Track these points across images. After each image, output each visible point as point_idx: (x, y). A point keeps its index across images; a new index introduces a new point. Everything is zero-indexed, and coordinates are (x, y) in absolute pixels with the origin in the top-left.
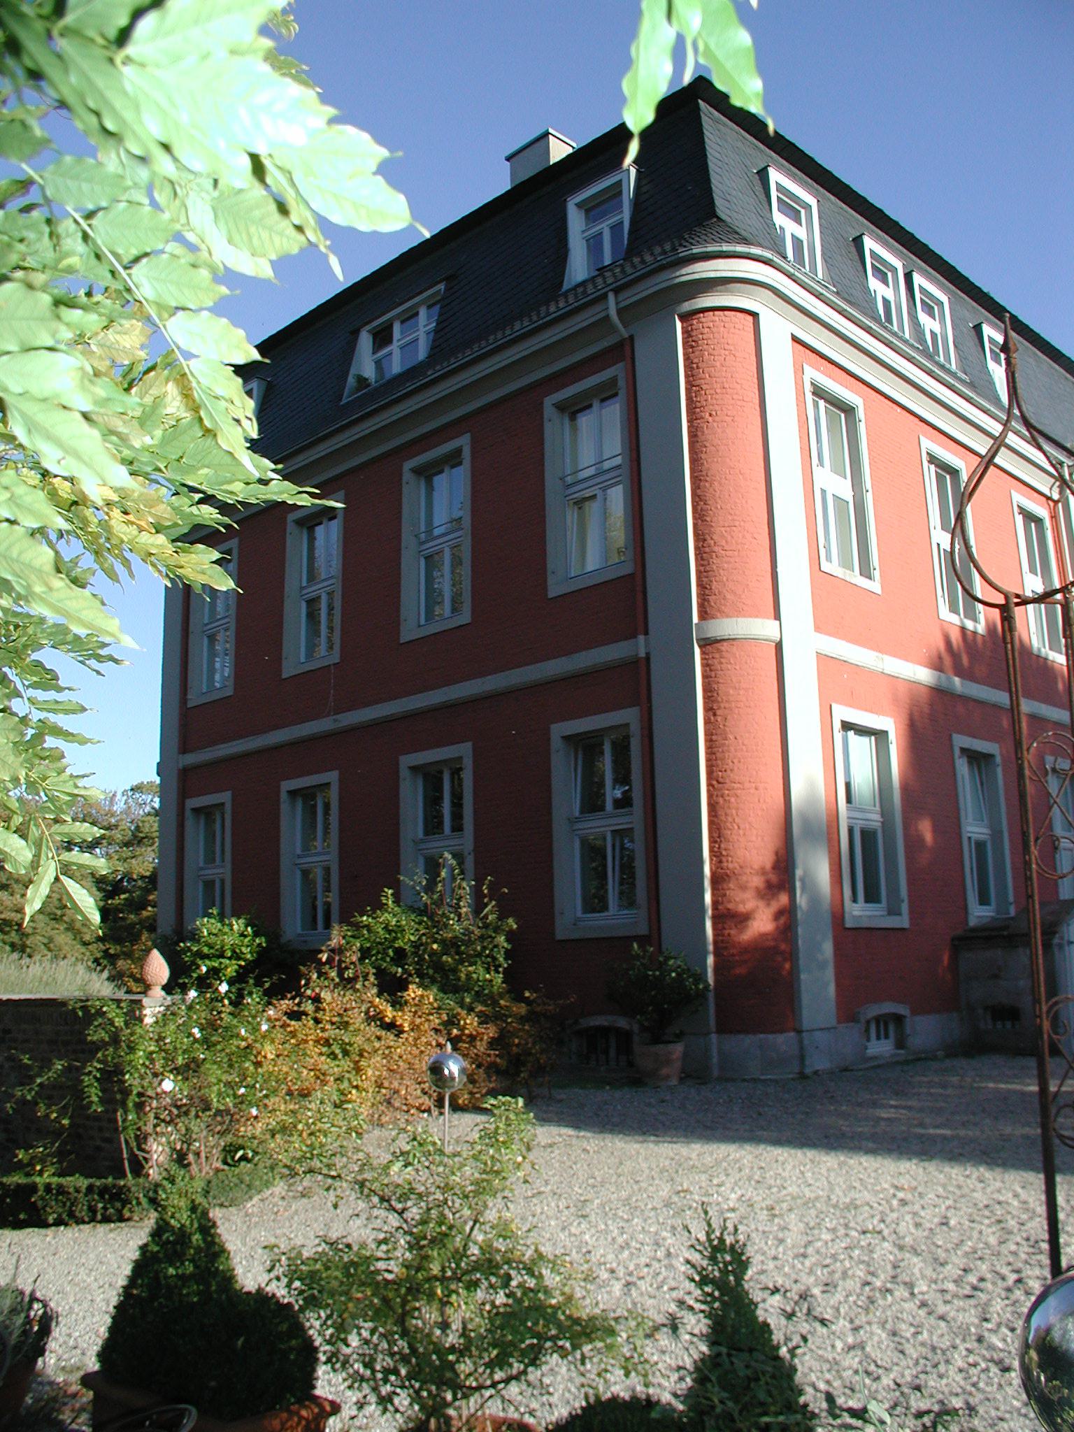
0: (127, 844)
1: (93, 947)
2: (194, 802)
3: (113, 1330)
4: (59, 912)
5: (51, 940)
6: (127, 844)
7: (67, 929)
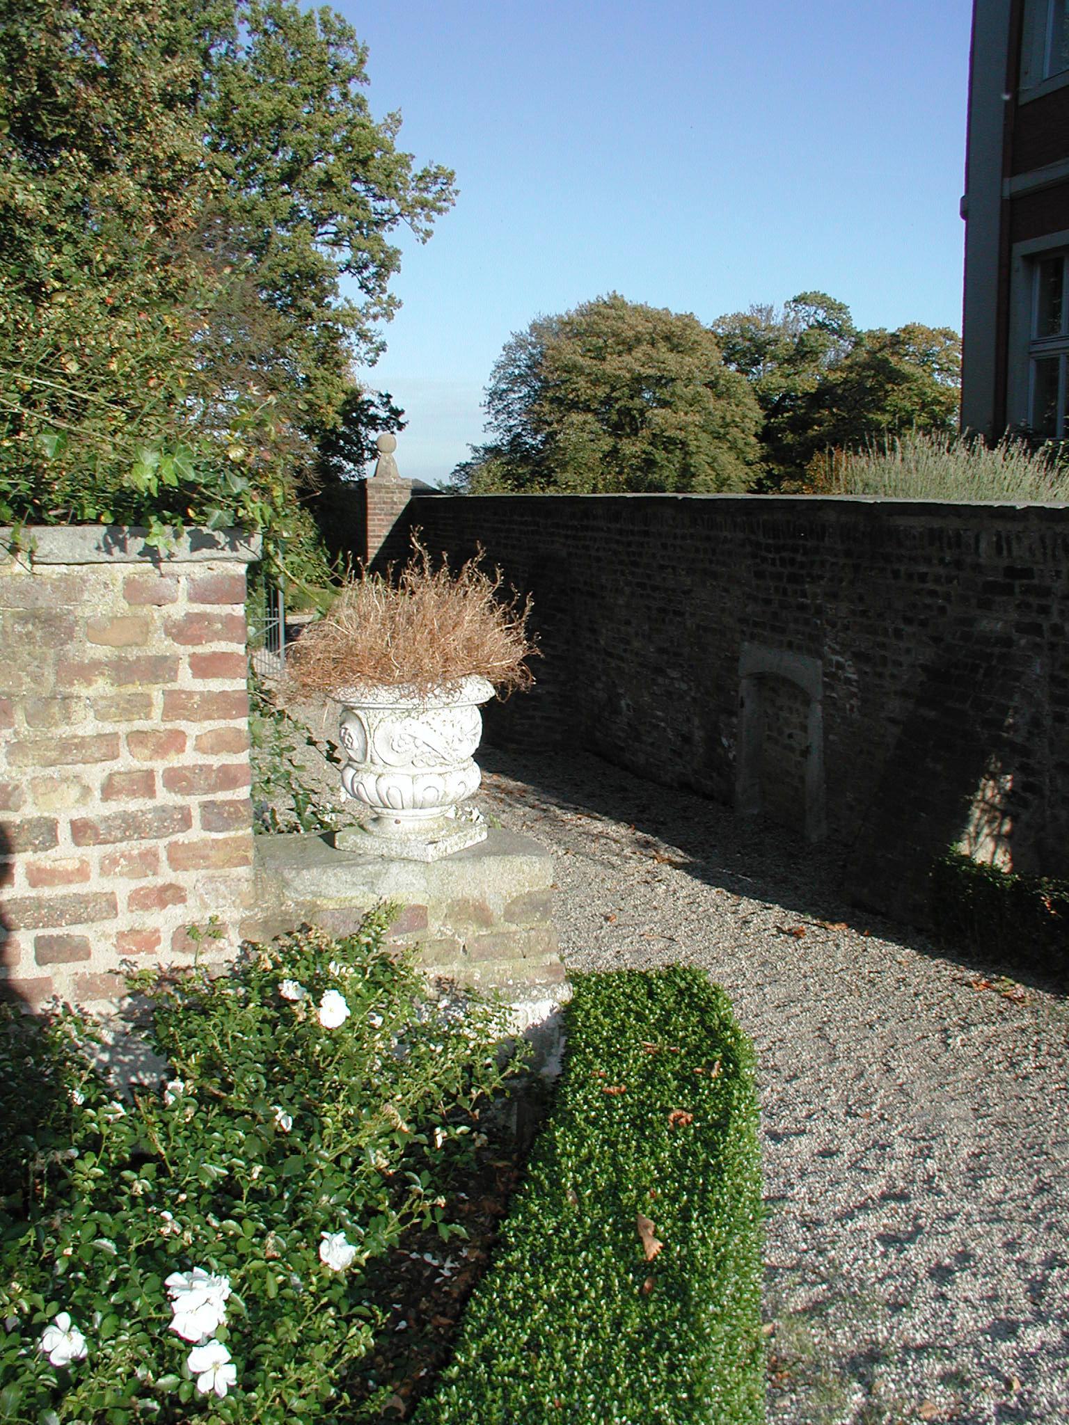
0: (790, 361)
1: (756, 467)
2: (1023, 248)
3: (903, 941)
4: (722, 431)
5: (715, 459)
6: (790, 361)
7: (730, 448)
